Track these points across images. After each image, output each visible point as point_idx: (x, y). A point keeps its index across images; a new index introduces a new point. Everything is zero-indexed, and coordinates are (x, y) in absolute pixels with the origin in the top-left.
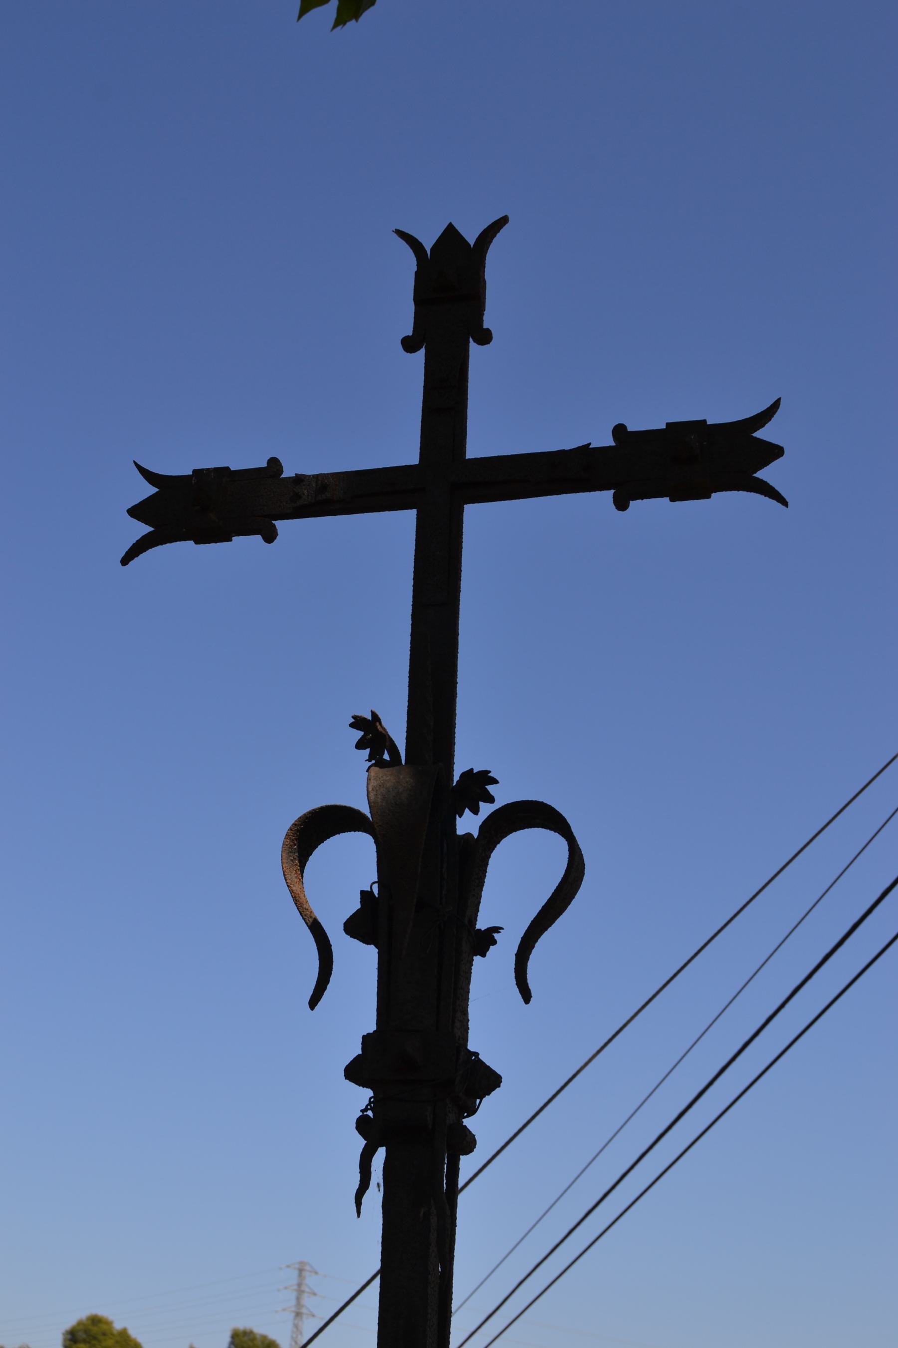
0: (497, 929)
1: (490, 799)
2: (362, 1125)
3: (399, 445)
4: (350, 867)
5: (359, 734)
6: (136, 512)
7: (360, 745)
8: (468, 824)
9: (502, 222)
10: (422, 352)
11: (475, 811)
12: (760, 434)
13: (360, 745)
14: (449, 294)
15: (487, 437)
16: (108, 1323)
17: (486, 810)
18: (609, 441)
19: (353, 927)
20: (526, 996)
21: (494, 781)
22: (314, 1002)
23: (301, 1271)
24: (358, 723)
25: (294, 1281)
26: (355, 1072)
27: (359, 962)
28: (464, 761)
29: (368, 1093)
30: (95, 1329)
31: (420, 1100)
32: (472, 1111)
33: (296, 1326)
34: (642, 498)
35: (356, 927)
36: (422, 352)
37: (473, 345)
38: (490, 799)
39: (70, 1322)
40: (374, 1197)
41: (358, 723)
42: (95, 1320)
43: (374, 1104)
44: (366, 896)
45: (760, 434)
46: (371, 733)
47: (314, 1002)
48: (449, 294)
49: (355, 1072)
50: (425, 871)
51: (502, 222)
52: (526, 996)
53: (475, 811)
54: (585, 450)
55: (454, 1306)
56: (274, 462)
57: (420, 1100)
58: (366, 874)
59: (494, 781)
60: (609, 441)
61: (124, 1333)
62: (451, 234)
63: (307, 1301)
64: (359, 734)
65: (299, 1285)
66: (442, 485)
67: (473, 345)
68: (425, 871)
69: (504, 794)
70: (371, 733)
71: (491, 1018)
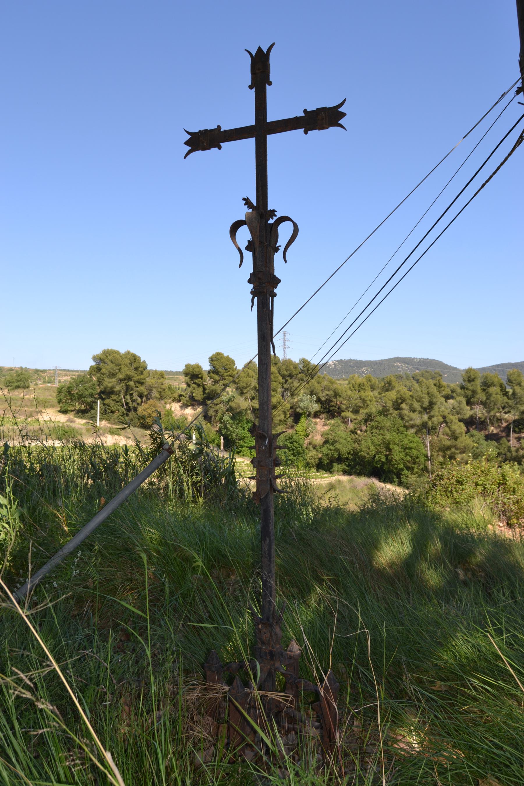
0: (280, 246)
1: (276, 216)
2: (252, 293)
3: (249, 119)
4: (244, 235)
5: (245, 202)
6: (186, 143)
7: (245, 204)
8: (271, 221)
9: (274, 44)
10: (254, 89)
11: (273, 219)
12: (340, 110)
13: (245, 204)
14: (260, 67)
15: (273, 115)
16: (223, 354)
17: (275, 218)
18: (303, 114)
19: (247, 248)
20: (286, 261)
21: (276, 211)
22: (240, 266)
23: (284, 334)
24: (244, 199)
25: (283, 337)
26: (250, 281)
27: (249, 256)
28: (270, 207)
29: (252, 285)
30: (218, 357)
31: (264, 285)
32: (276, 287)
33: (284, 351)
34: (311, 130)
35: (247, 248)
36: (254, 89)
37: (267, 86)
38: (276, 216)
39: (210, 355)
40: (255, 308)
41: (244, 199)
42: (218, 354)
43: (254, 288)
44: (249, 241)
45: (340, 110)
46: (247, 202)
47: (240, 266)
48: (260, 67)
49: (250, 281)
50: (263, 233)
51: (274, 44)
52: (286, 261)
53: (273, 219)
54: (297, 118)
55: (276, 328)
56: (219, 127)
57: (264, 285)
58: (249, 237)
59: (276, 211)
60: (303, 114)
61: (228, 357)
62: (260, 49)
63: (287, 343)
64: (245, 202)
65: (284, 338)
66: (261, 130)
67: (267, 86)
68: (263, 233)
69: (279, 215)
70: (247, 202)
71: (279, 267)
